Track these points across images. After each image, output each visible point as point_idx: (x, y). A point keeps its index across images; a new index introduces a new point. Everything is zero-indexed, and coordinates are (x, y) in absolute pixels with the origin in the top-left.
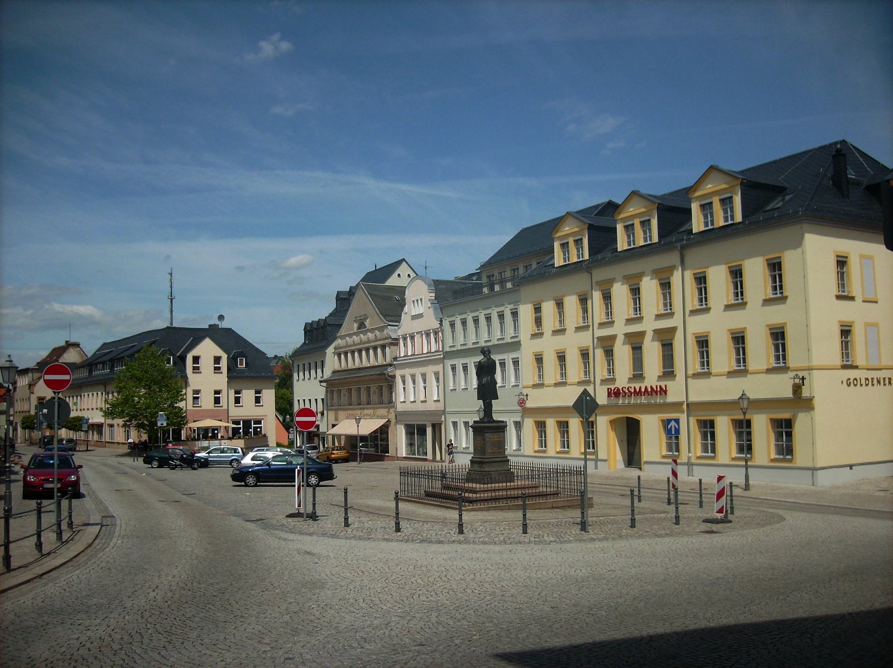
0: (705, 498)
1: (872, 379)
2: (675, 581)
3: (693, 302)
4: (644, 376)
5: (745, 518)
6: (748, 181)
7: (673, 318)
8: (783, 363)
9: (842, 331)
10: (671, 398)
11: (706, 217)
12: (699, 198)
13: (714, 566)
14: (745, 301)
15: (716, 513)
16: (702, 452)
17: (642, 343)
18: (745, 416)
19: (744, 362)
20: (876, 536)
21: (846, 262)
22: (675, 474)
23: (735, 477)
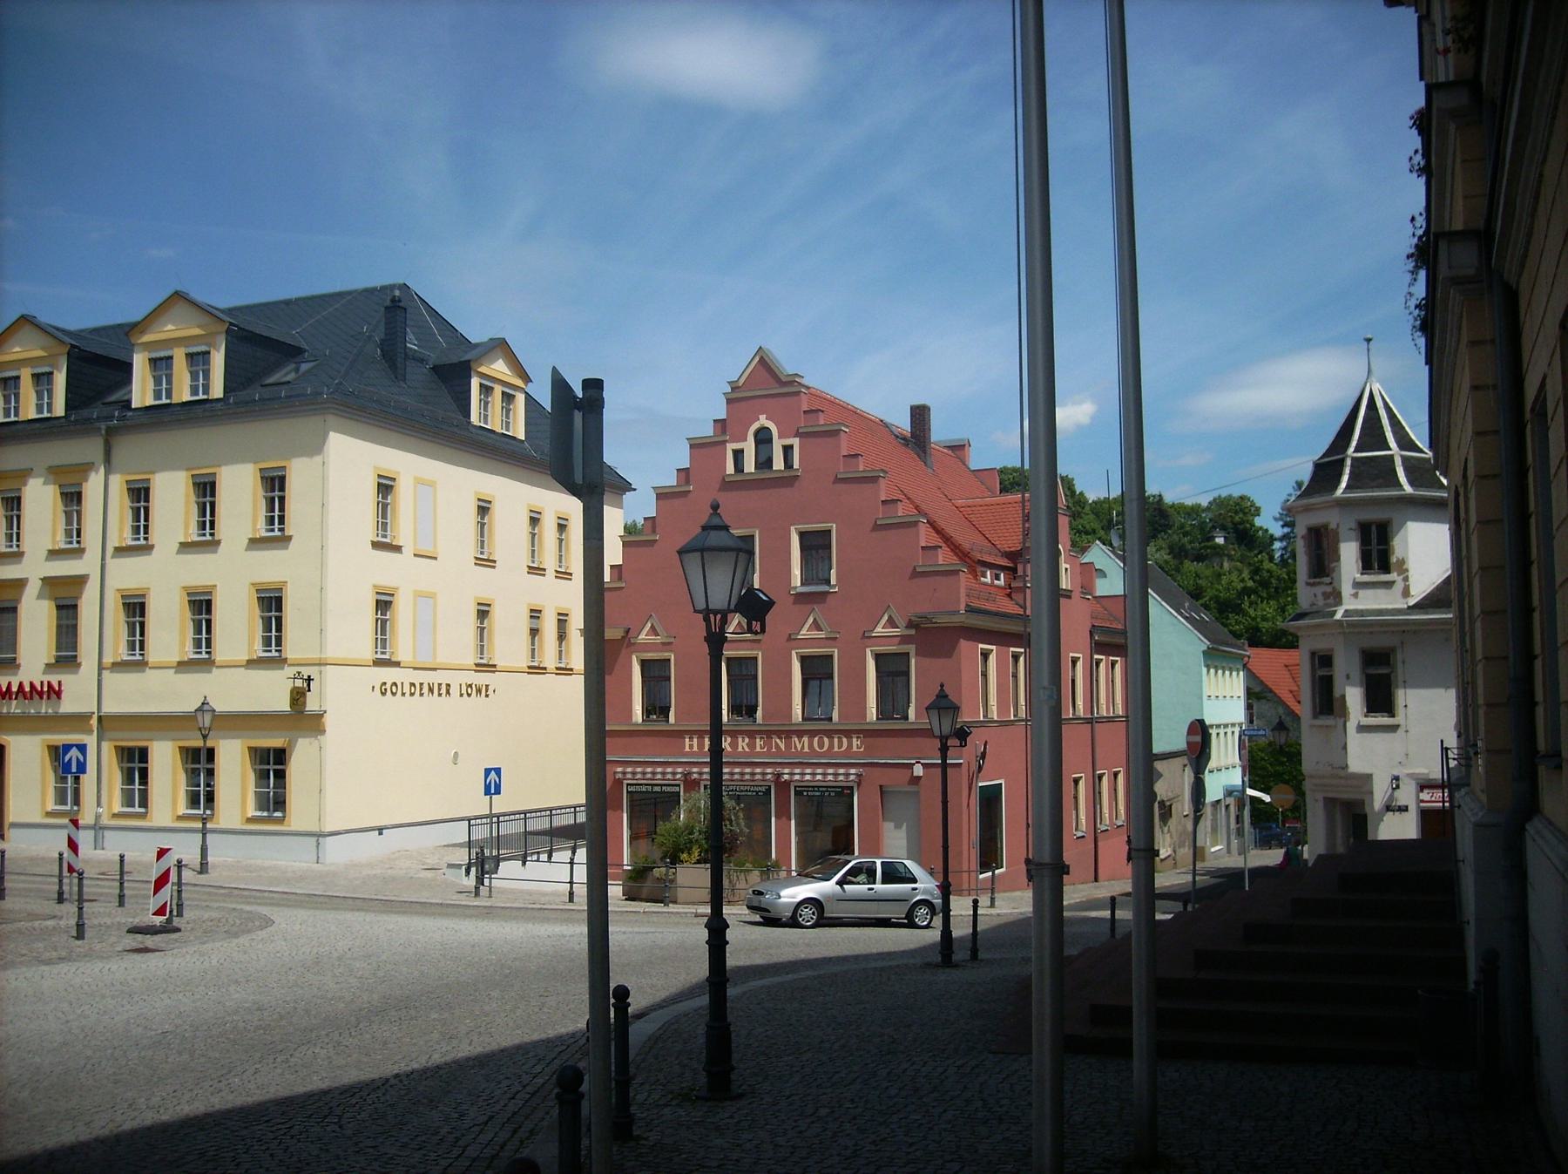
0: (129, 888)
1: (421, 684)
2: (86, 1043)
3: (120, 532)
4: (18, 663)
5: (204, 922)
6: (240, 328)
7: (81, 558)
8: (207, 653)
9: (378, 602)
10: (67, 706)
11: (158, 381)
12: (148, 346)
13: (154, 1011)
14: (216, 538)
15: (153, 914)
16: (56, 804)
17: (18, 600)
18: (205, 741)
19: (209, 645)
20: (424, 944)
21: (392, 486)
22: (73, 846)
23: (185, 849)
